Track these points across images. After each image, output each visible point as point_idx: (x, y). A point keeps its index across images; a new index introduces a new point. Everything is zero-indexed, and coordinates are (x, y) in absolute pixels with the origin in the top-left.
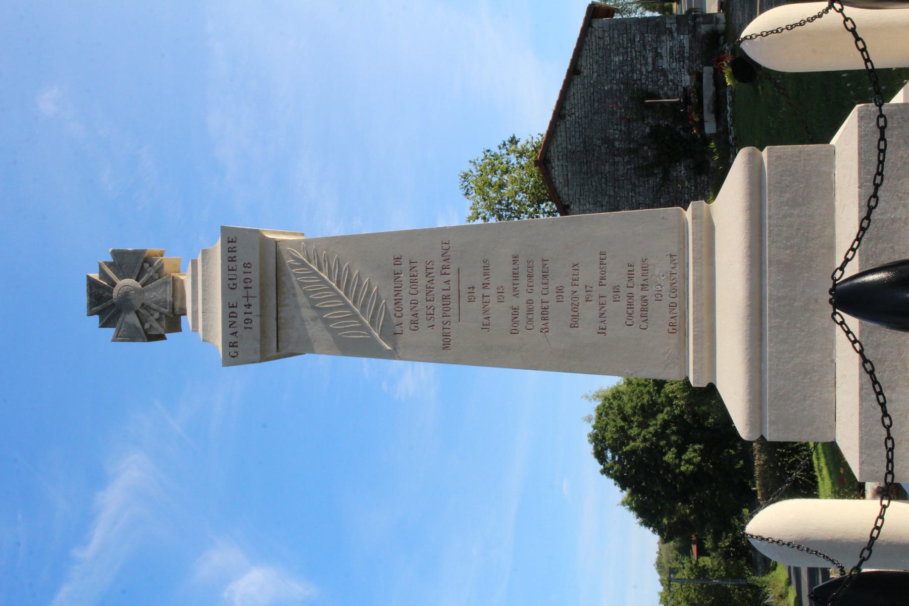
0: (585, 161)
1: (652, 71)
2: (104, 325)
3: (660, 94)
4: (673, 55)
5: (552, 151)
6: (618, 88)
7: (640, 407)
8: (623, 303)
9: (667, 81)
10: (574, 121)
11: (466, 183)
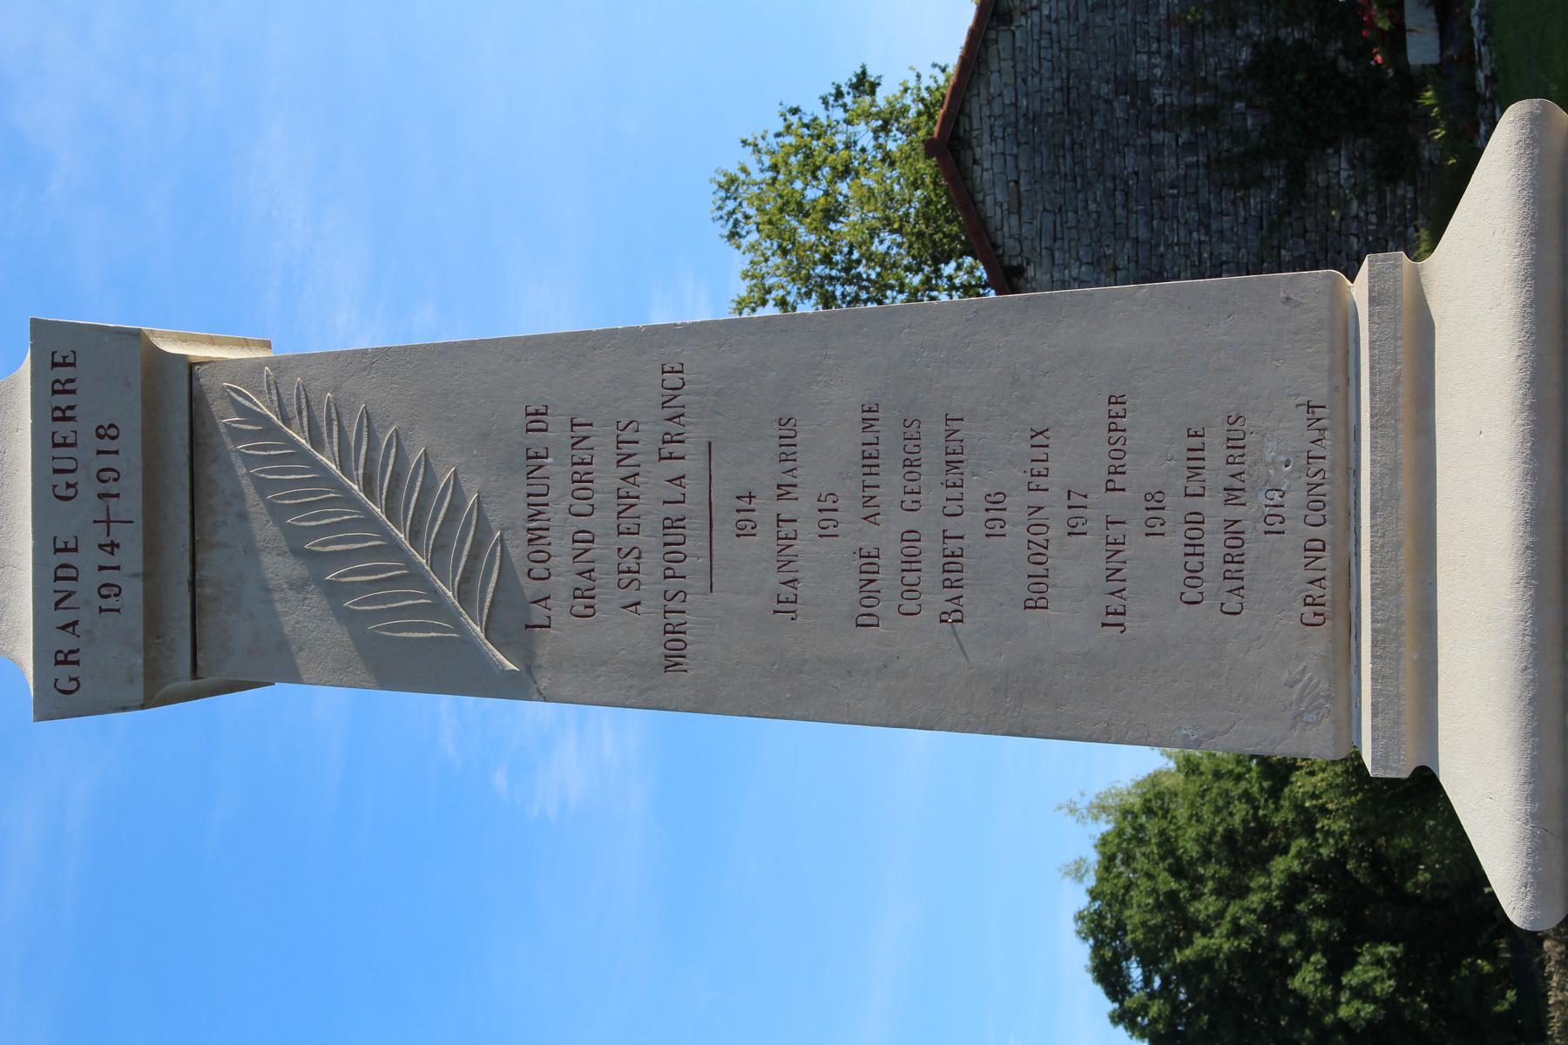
7: (1223, 837)
8: (1175, 542)
10: (1036, 31)
11: (731, 205)
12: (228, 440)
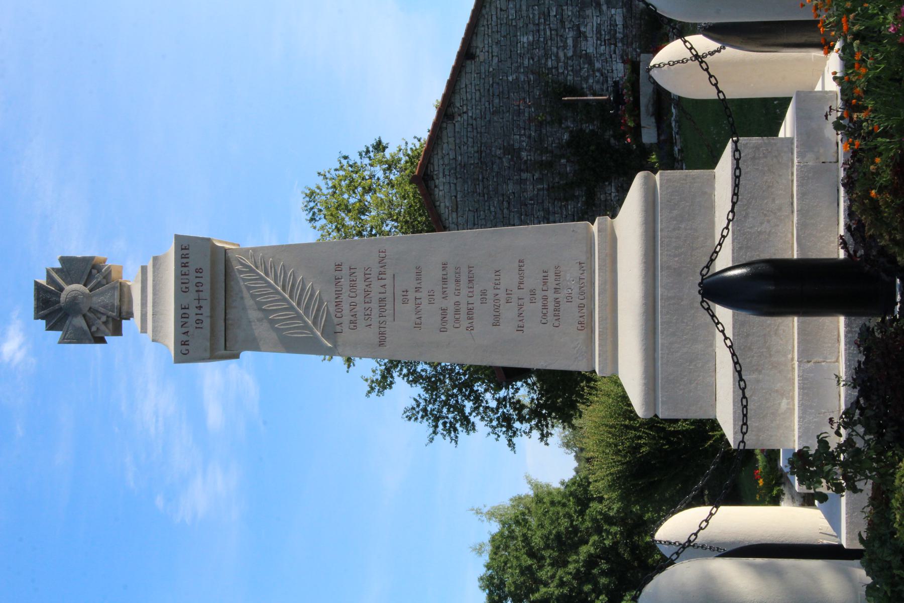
0: (480, 178)
1: (572, 56)
2: (50, 328)
3: (583, 88)
4: (601, 35)
5: (436, 163)
6: (526, 79)
7: (555, 535)
8: (539, 304)
9: (593, 71)
10: (465, 123)
11: (312, 204)
12: (237, 274)
